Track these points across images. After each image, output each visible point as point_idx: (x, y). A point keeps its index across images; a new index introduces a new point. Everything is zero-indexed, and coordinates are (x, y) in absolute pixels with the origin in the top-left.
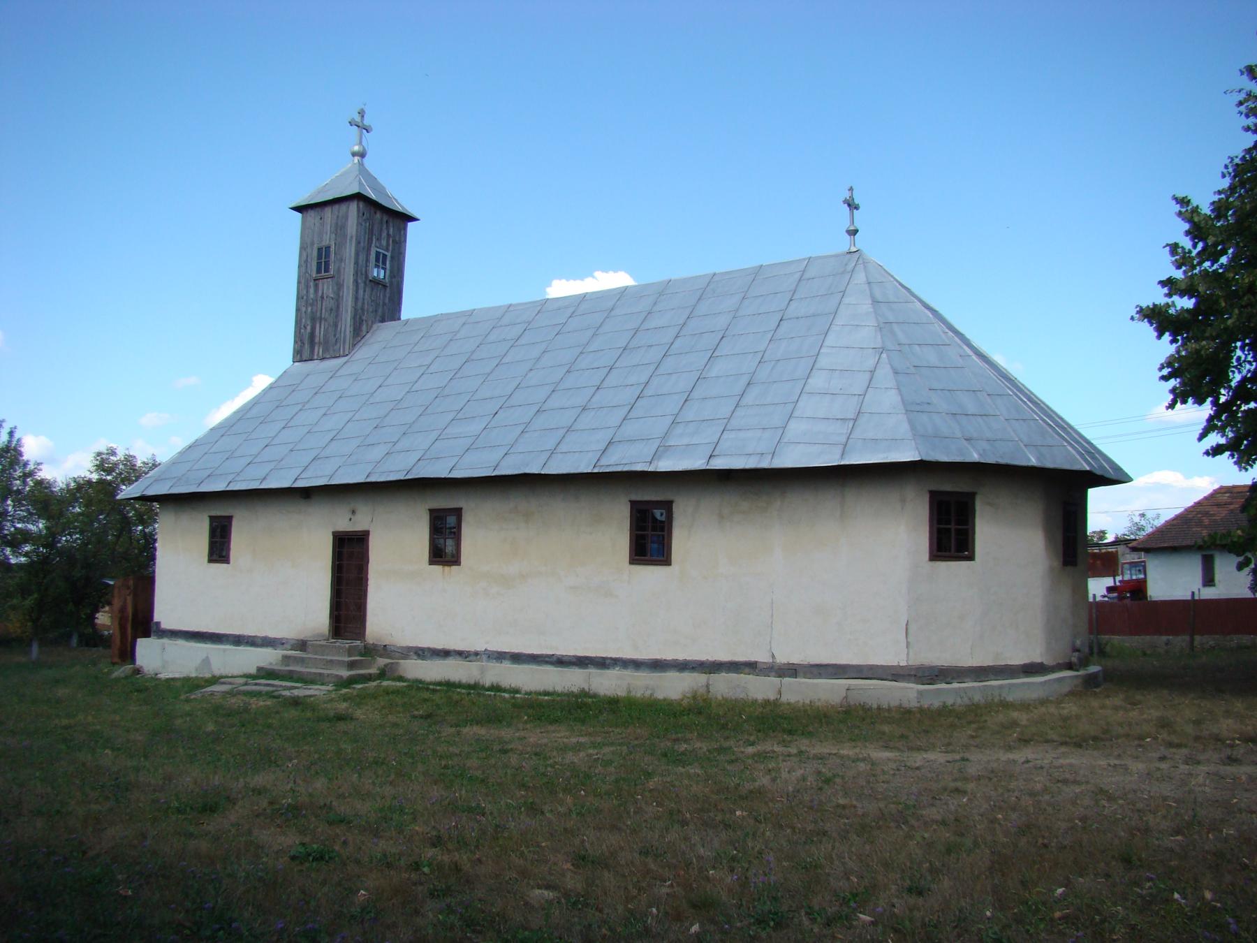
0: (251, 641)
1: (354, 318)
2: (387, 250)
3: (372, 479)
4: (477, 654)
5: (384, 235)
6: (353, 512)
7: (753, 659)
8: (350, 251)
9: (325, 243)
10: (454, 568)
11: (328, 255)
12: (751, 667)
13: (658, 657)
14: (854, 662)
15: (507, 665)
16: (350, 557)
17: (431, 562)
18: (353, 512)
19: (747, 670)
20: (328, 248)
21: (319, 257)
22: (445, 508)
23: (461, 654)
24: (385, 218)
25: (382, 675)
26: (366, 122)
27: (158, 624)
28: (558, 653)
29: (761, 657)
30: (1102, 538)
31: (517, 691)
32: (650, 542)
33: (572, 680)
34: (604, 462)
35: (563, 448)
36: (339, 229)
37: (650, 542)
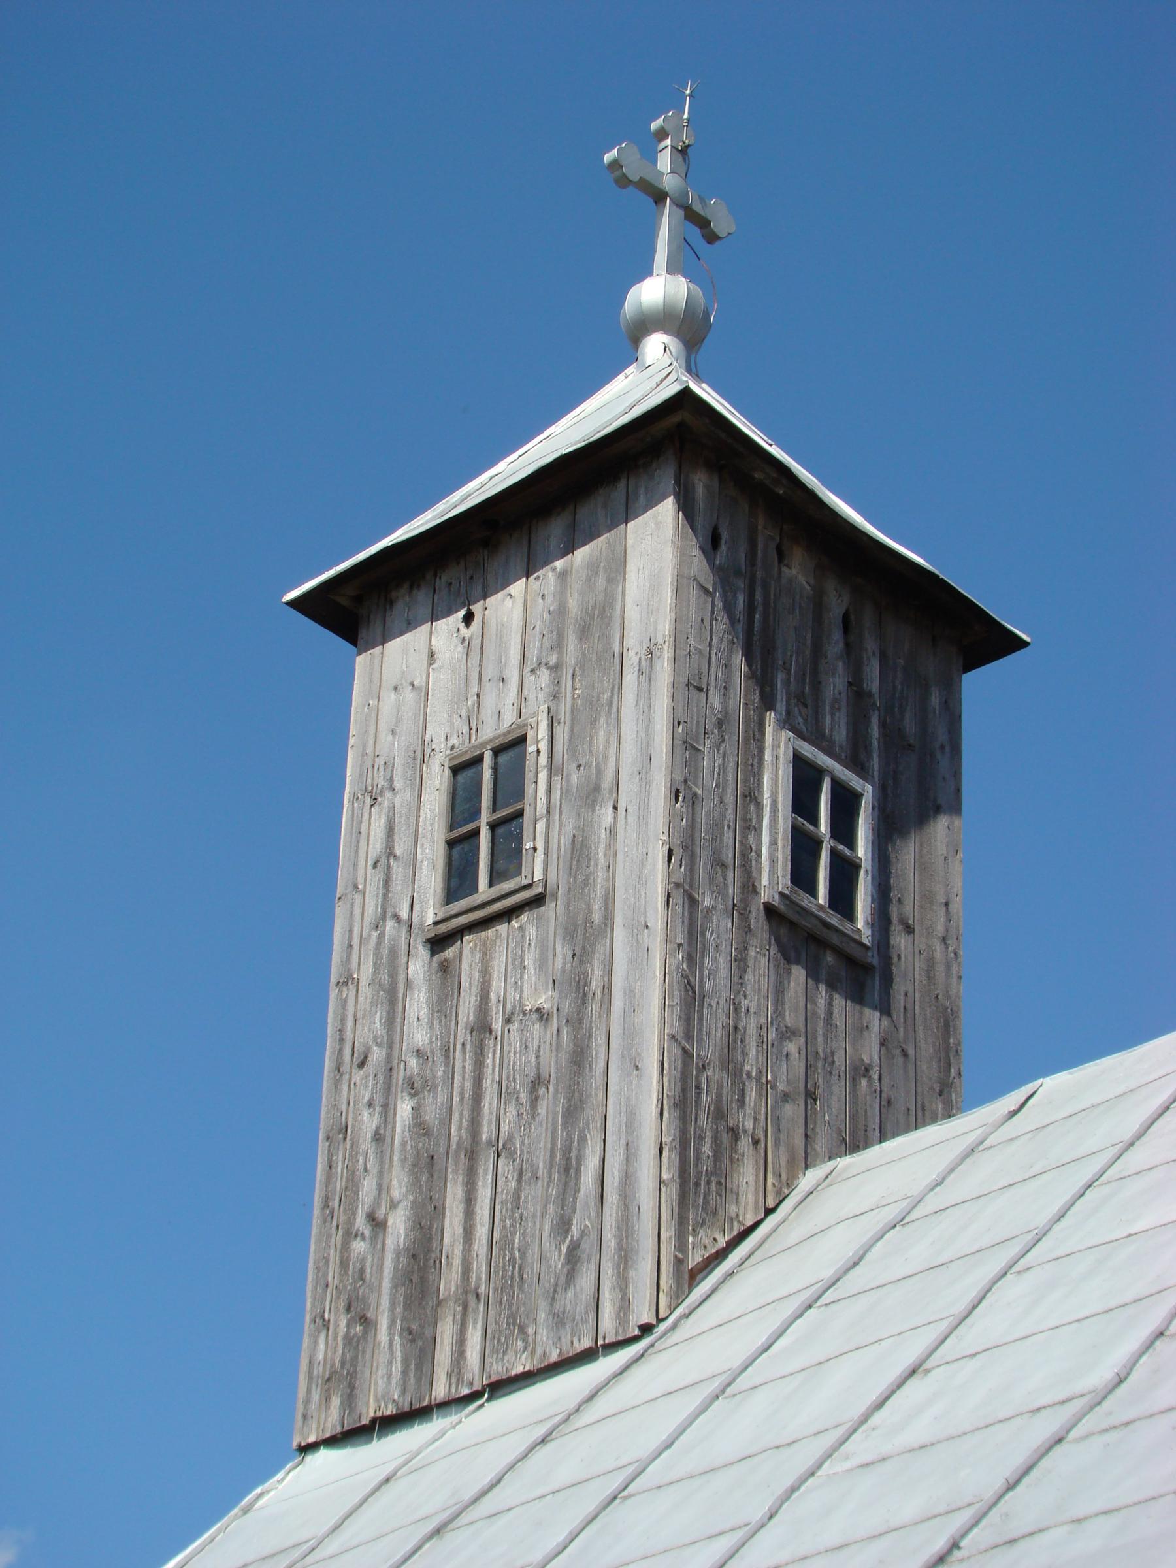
1: (682, 1102)
5: (835, 684)
11: (510, 785)
21: (462, 806)
24: (837, 603)
30: (787, 566)
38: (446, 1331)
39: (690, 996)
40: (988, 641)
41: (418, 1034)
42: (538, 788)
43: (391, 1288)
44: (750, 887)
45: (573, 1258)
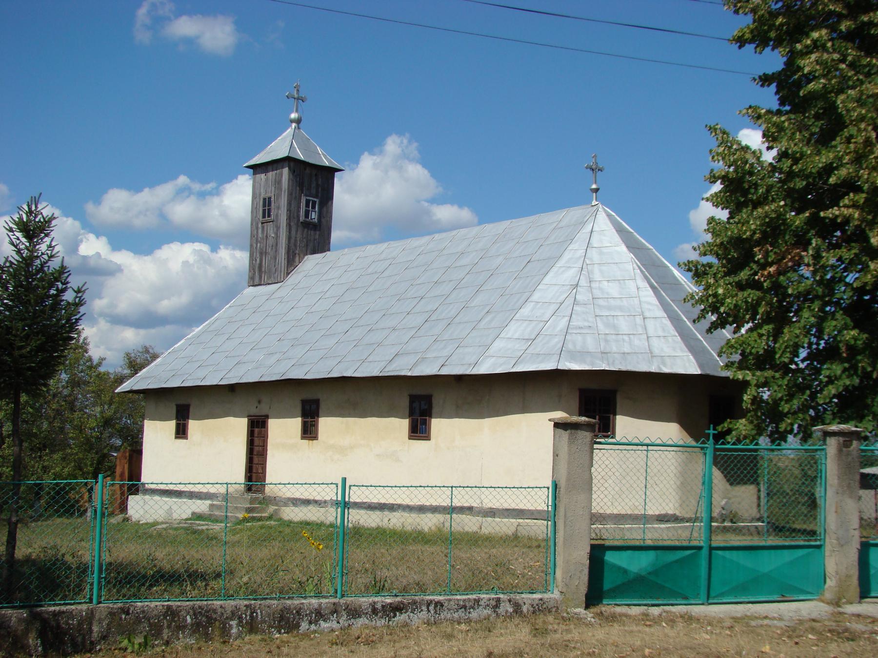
0: (192, 495)
2: (316, 197)
3: (263, 380)
5: (314, 185)
6: (259, 402)
8: (284, 201)
16: (257, 431)
17: (303, 438)
18: (259, 402)
19: (467, 512)
21: (264, 206)
22: (313, 400)
23: (315, 502)
25: (270, 518)
26: (302, 95)
34: (386, 370)
35: (371, 358)
36: (278, 182)
37: (419, 430)
39: (289, 238)
41: (260, 235)
44: (299, 220)
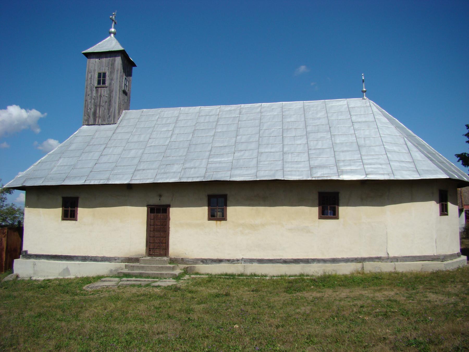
4: (238, 260)
6: (160, 196)
7: (379, 256)
9: (102, 71)
10: (222, 222)
12: (379, 259)
13: (335, 257)
14: (418, 255)
15: (256, 265)
17: (209, 219)
19: (377, 260)
20: (104, 74)
23: (228, 261)
27: (26, 252)
28: (283, 258)
29: (383, 255)
31: (266, 276)
32: (70, 215)
33: (295, 270)
37: (70, 215)
38: (97, 119)
40: (135, 66)
42: (107, 78)
43: (168, 286)
45: (109, 116)
